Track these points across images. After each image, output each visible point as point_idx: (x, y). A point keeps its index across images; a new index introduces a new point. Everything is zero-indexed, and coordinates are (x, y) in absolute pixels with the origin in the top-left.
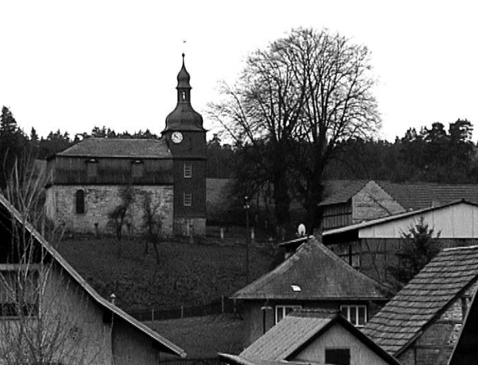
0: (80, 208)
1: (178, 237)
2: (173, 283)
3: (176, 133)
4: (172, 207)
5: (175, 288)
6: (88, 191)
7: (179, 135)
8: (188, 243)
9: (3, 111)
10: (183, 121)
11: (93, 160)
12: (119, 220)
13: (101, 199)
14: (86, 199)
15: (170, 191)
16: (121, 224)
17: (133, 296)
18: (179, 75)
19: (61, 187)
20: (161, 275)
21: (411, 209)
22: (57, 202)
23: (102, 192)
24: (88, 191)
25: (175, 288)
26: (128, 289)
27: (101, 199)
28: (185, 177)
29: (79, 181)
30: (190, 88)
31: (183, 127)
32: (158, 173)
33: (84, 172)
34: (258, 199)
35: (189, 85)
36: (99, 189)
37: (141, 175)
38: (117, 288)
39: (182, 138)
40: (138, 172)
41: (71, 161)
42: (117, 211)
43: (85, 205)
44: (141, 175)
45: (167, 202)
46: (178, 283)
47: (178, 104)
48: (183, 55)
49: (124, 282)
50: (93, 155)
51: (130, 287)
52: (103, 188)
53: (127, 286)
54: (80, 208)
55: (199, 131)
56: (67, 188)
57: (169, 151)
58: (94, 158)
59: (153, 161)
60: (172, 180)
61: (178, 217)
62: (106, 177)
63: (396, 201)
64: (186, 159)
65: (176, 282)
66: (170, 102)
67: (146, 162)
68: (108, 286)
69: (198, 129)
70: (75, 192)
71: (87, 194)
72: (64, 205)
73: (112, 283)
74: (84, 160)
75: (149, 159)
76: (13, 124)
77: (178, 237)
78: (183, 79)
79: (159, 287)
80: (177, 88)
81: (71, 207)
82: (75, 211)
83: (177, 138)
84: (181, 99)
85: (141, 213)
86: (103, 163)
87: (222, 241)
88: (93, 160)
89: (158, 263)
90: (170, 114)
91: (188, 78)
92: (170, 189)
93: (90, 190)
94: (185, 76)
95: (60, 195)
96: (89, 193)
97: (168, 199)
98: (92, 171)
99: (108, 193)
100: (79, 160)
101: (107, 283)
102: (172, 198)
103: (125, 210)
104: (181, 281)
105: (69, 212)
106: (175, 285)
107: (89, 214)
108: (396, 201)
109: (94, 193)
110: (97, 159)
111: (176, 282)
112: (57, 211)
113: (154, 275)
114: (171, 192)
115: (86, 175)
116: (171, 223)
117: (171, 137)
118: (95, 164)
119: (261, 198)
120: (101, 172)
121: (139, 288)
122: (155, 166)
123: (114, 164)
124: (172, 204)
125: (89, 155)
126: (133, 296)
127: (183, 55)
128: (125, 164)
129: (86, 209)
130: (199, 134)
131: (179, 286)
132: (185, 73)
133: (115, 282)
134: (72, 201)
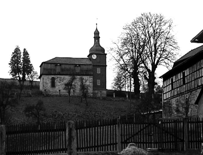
0: (53, 85)
1: (95, 97)
2: (94, 114)
3: (94, 55)
4: (92, 85)
5: (95, 116)
6: (56, 78)
7: (95, 56)
8: (100, 99)
9: (24, 50)
10: (97, 50)
11: (59, 65)
12: (70, 87)
13: (62, 81)
14: (56, 81)
15: (91, 78)
16: (71, 88)
17: (75, 119)
18: (95, 32)
19: (45, 76)
20: (88, 111)
21: (161, 102)
22: (43, 82)
23: (63, 78)
24: (56, 78)
25: (95, 116)
26: (73, 116)
27: (62, 81)
28: (98, 73)
29: (53, 73)
30: (99, 37)
31: (98, 52)
32: (87, 71)
33: (55, 70)
34: (125, 88)
35: (99, 36)
36: (61, 77)
37: (79, 71)
38: (68, 115)
39: (96, 57)
40: (78, 70)
41: (49, 65)
42: (69, 83)
43: (55, 84)
44: (79, 71)
45: (90, 83)
46: (96, 114)
47: (94, 44)
48: (97, 24)
49: (71, 113)
50: (59, 63)
51: (74, 115)
52: (63, 77)
53: (72, 115)
54: (53, 85)
55: (103, 54)
56: (47, 76)
57: (91, 62)
58: (59, 64)
59: (84, 66)
60: (92, 73)
61: (95, 90)
62: (63, 72)
63: (71, 148)
64: (99, 66)
65: (95, 114)
66: (91, 43)
67: (81, 66)
68: (64, 115)
69: (103, 53)
70: (51, 78)
71: (56, 79)
72: (47, 83)
73: (66, 113)
74: (55, 65)
75: (83, 65)
76: (28, 55)
77: (95, 97)
78: (97, 34)
79: (88, 116)
80: (94, 37)
81: (50, 84)
82: (51, 86)
83: (94, 57)
84: (95, 41)
85: (79, 83)
86: (63, 66)
87: (114, 99)
88: (59, 65)
89: (87, 105)
90: (91, 48)
91: (99, 33)
92: (92, 77)
93: (57, 77)
94: (98, 32)
95: (45, 79)
96: (57, 78)
97: (91, 82)
98: (58, 69)
99: (65, 79)
100: (53, 65)
101: (64, 113)
102: (92, 81)
103: (72, 83)
104: (98, 113)
105: (48, 86)
106: (95, 115)
107: (57, 87)
108: (71, 148)
109: (59, 79)
110: (61, 64)
111: (95, 114)
112: (43, 86)
113: (85, 111)
114: (92, 79)
115: (56, 71)
116: (92, 92)
117: (91, 57)
118: (60, 66)
119: (126, 88)
120: (62, 70)
121: (78, 116)
122: (85, 68)
123: (67, 67)
124: (92, 84)
125: (57, 63)
126: (75, 119)
127: (97, 24)
128: (72, 67)
129: (55, 85)
130: (102, 55)
131: (97, 115)
132: (97, 31)
133: (67, 113)
134: (50, 81)
